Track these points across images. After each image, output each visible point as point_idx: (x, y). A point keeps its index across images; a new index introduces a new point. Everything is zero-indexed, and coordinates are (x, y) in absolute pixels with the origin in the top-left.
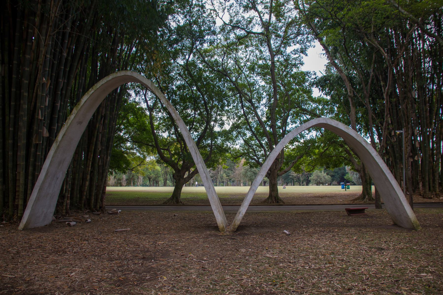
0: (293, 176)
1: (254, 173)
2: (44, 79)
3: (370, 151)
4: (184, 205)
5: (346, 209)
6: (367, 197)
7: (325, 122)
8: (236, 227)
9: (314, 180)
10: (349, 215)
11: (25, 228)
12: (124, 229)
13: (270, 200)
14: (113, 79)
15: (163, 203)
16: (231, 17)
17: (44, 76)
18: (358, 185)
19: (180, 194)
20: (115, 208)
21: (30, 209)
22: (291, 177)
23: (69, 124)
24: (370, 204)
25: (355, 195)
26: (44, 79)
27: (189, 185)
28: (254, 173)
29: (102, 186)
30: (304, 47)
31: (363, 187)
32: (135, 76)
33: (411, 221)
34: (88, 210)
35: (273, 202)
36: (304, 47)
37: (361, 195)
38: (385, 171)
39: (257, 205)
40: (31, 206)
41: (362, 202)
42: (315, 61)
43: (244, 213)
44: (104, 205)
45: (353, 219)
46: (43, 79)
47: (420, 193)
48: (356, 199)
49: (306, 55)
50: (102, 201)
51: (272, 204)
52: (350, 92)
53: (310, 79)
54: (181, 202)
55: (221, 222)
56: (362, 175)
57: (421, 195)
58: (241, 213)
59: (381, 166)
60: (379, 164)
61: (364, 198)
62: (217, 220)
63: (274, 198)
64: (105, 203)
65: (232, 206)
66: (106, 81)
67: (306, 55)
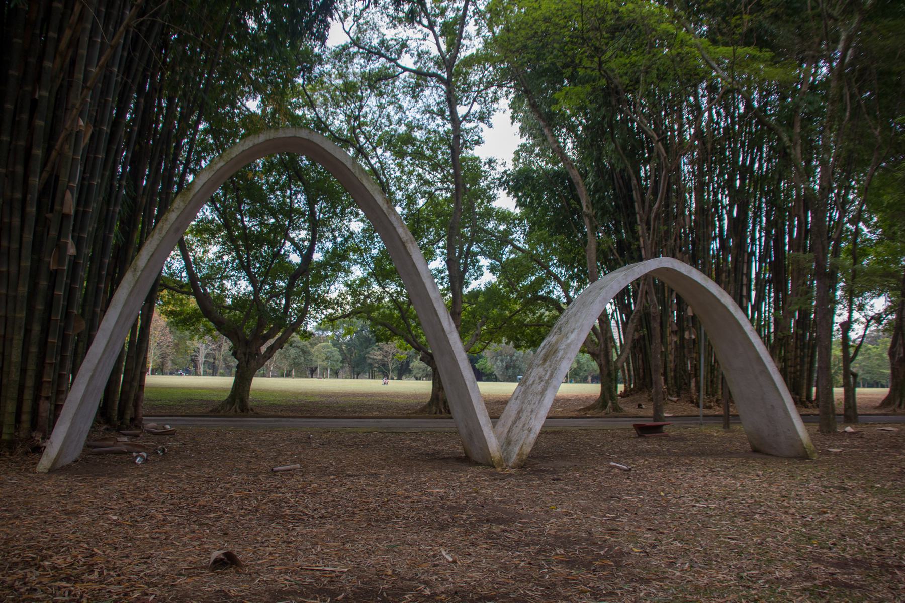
0: (373, 359)
1: (302, 350)
2: (81, 123)
3: (740, 322)
4: (257, 415)
5: (635, 425)
6: (610, 404)
7: (670, 266)
8: (525, 457)
9: (420, 369)
10: (640, 436)
11: (52, 471)
12: (288, 467)
13: (434, 408)
14: (267, 141)
15: (211, 411)
16: (360, 32)
17: (81, 115)
18: (504, 381)
19: (249, 391)
20: (155, 420)
21: (68, 424)
22: (369, 361)
23: (164, 232)
24: (616, 417)
25: (588, 398)
26: (81, 123)
27: (264, 376)
28: (302, 350)
29: (138, 372)
30: (485, 110)
31: (602, 387)
32: (318, 142)
33: (802, 444)
34: (105, 427)
35: (441, 412)
36: (485, 110)
37: (598, 401)
38: (764, 359)
39: (410, 418)
40: (71, 416)
41: (603, 413)
42: (500, 140)
43: (538, 431)
44: (141, 415)
45: (644, 445)
46: (78, 121)
47: (691, 398)
48: (588, 408)
49: (490, 126)
50: (136, 406)
51: (439, 415)
52: (587, 206)
53: (493, 172)
54: (252, 409)
55: (495, 449)
56: (603, 362)
57: (692, 402)
58: (533, 430)
59: (758, 349)
60: (756, 345)
61: (604, 406)
62: (489, 445)
63: (239, 400)
64: (142, 411)
65: (361, 418)
66: (251, 145)
67: (490, 126)
